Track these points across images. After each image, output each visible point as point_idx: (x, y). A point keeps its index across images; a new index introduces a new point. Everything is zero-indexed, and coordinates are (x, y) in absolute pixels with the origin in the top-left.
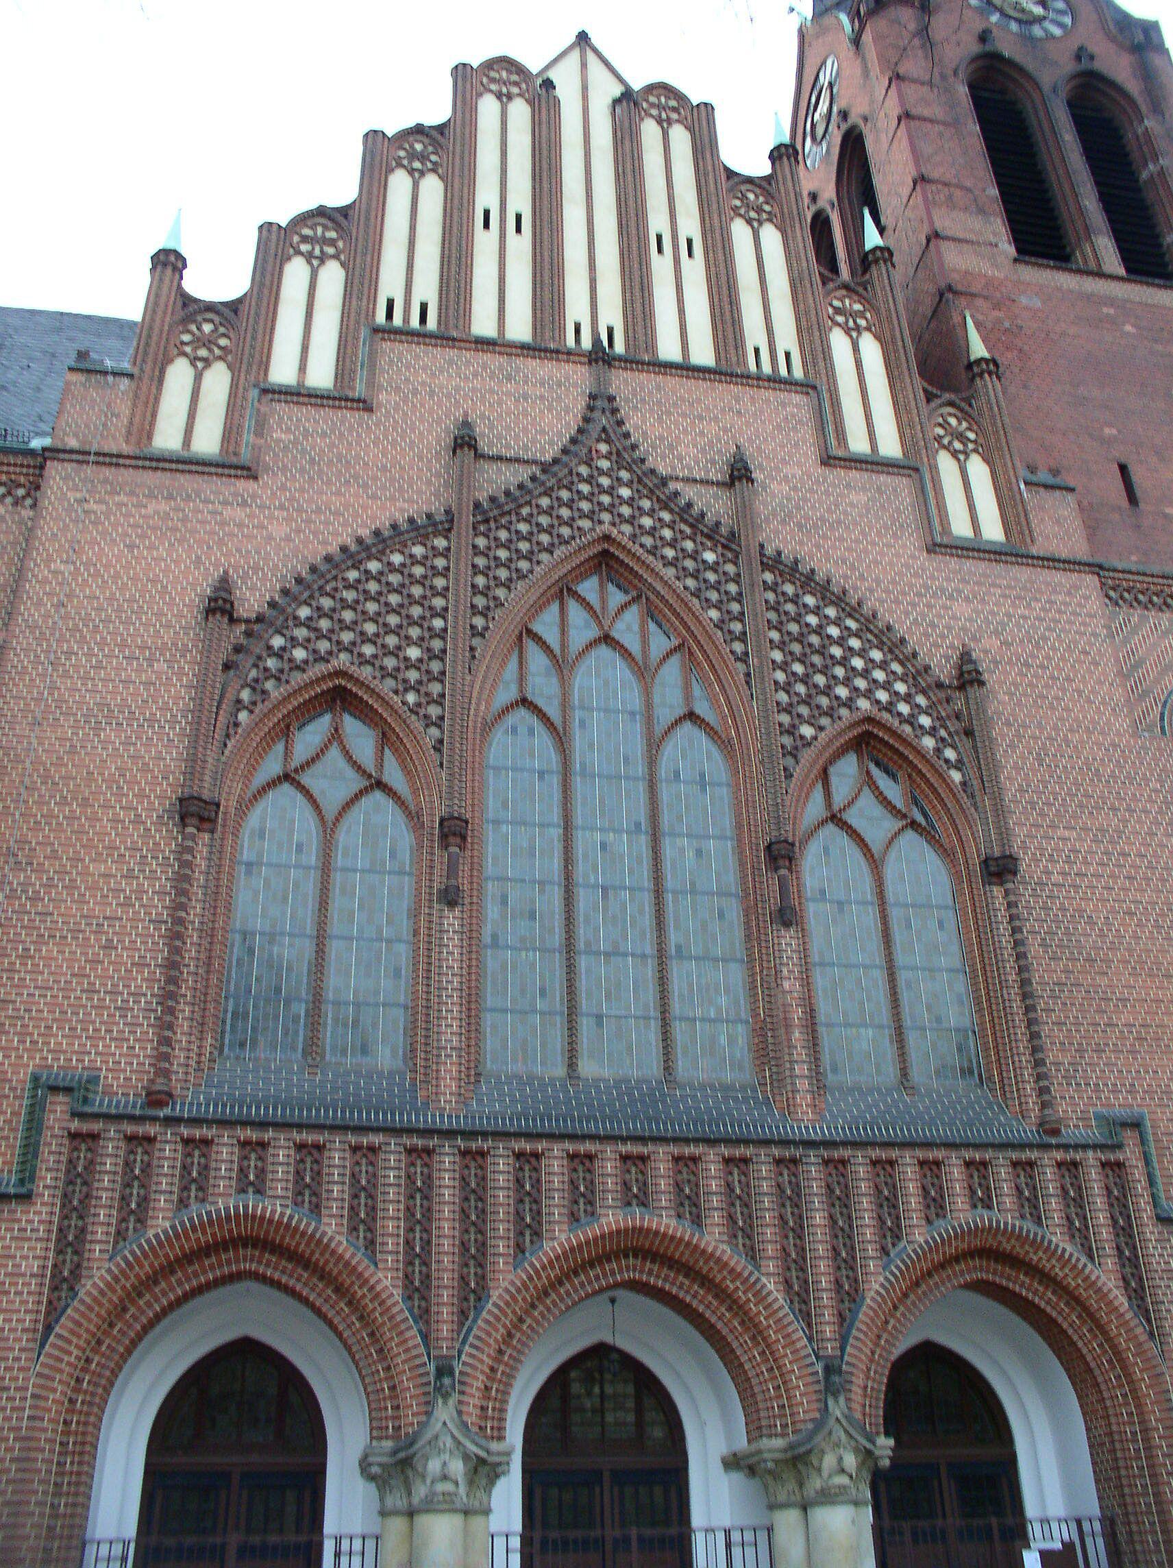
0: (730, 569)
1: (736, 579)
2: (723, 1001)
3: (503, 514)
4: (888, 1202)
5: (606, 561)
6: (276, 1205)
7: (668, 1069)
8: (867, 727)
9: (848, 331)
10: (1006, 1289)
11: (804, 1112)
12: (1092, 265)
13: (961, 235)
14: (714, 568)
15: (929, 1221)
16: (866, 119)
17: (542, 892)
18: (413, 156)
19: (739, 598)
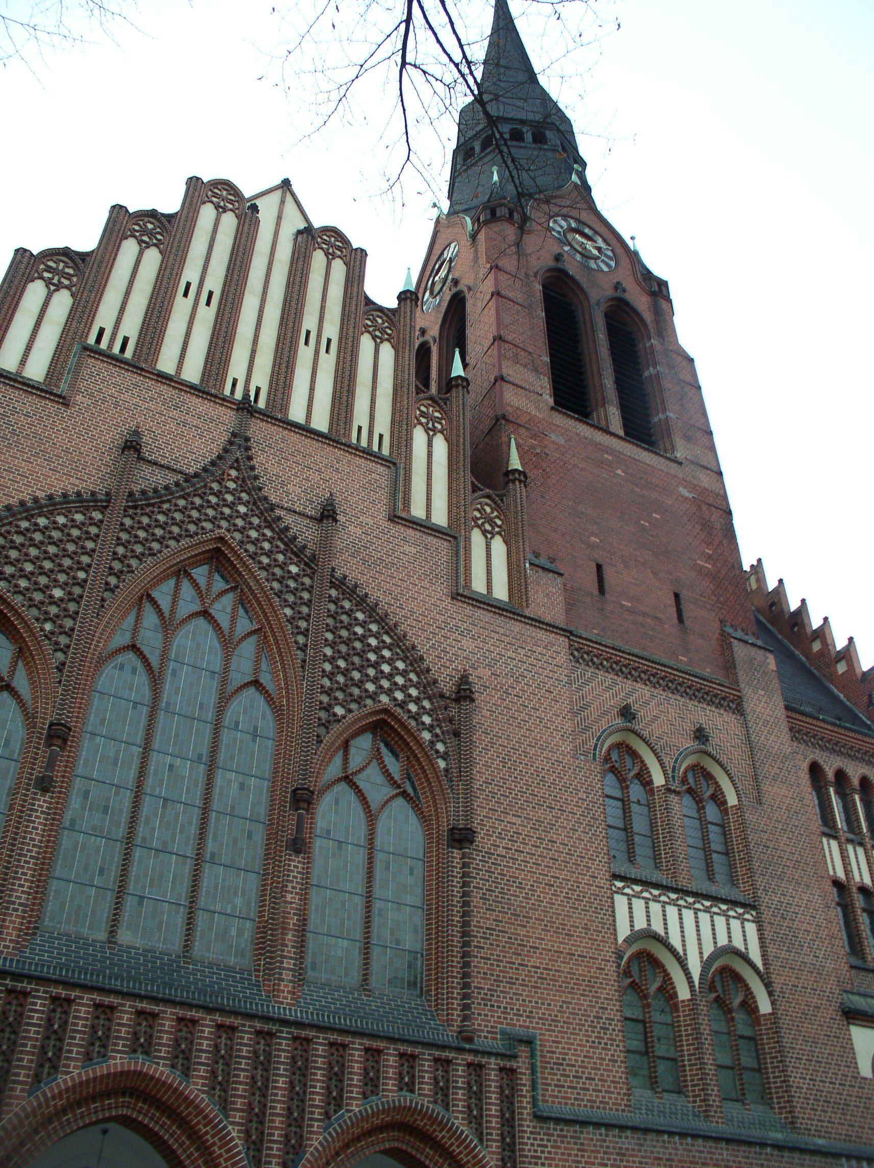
0: (307, 581)
1: (309, 590)
2: (239, 901)
3: (149, 505)
4: (336, 1076)
5: (217, 557)
7: (187, 947)
8: (382, 716)
9: (427, 430)
10: (414, 1157)
11: (286, 997)
12: (603, 424)
13: (518, 382)
14: (295, 578)
15: (365, 1096)
16: (470, 289)
17: (117, 793)
18: (144, 231)
19: (308, 604)
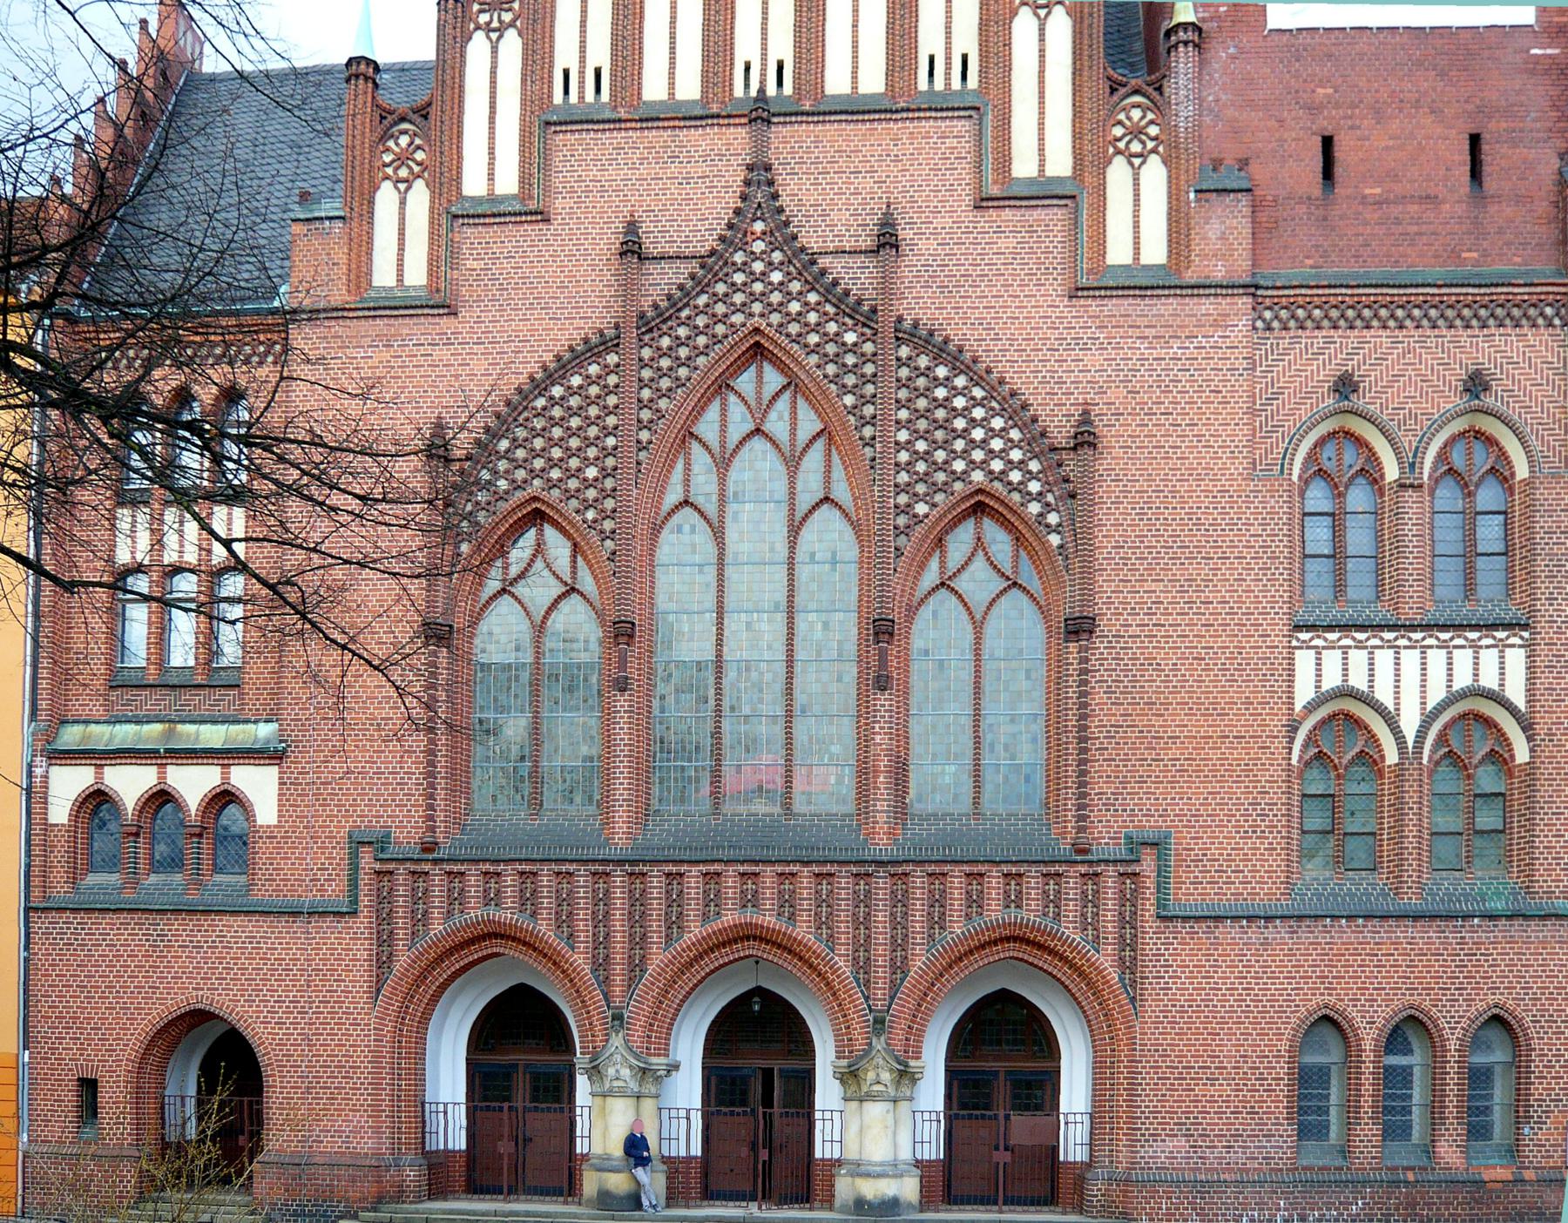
3: (664, 321)
6: (507, 913)
